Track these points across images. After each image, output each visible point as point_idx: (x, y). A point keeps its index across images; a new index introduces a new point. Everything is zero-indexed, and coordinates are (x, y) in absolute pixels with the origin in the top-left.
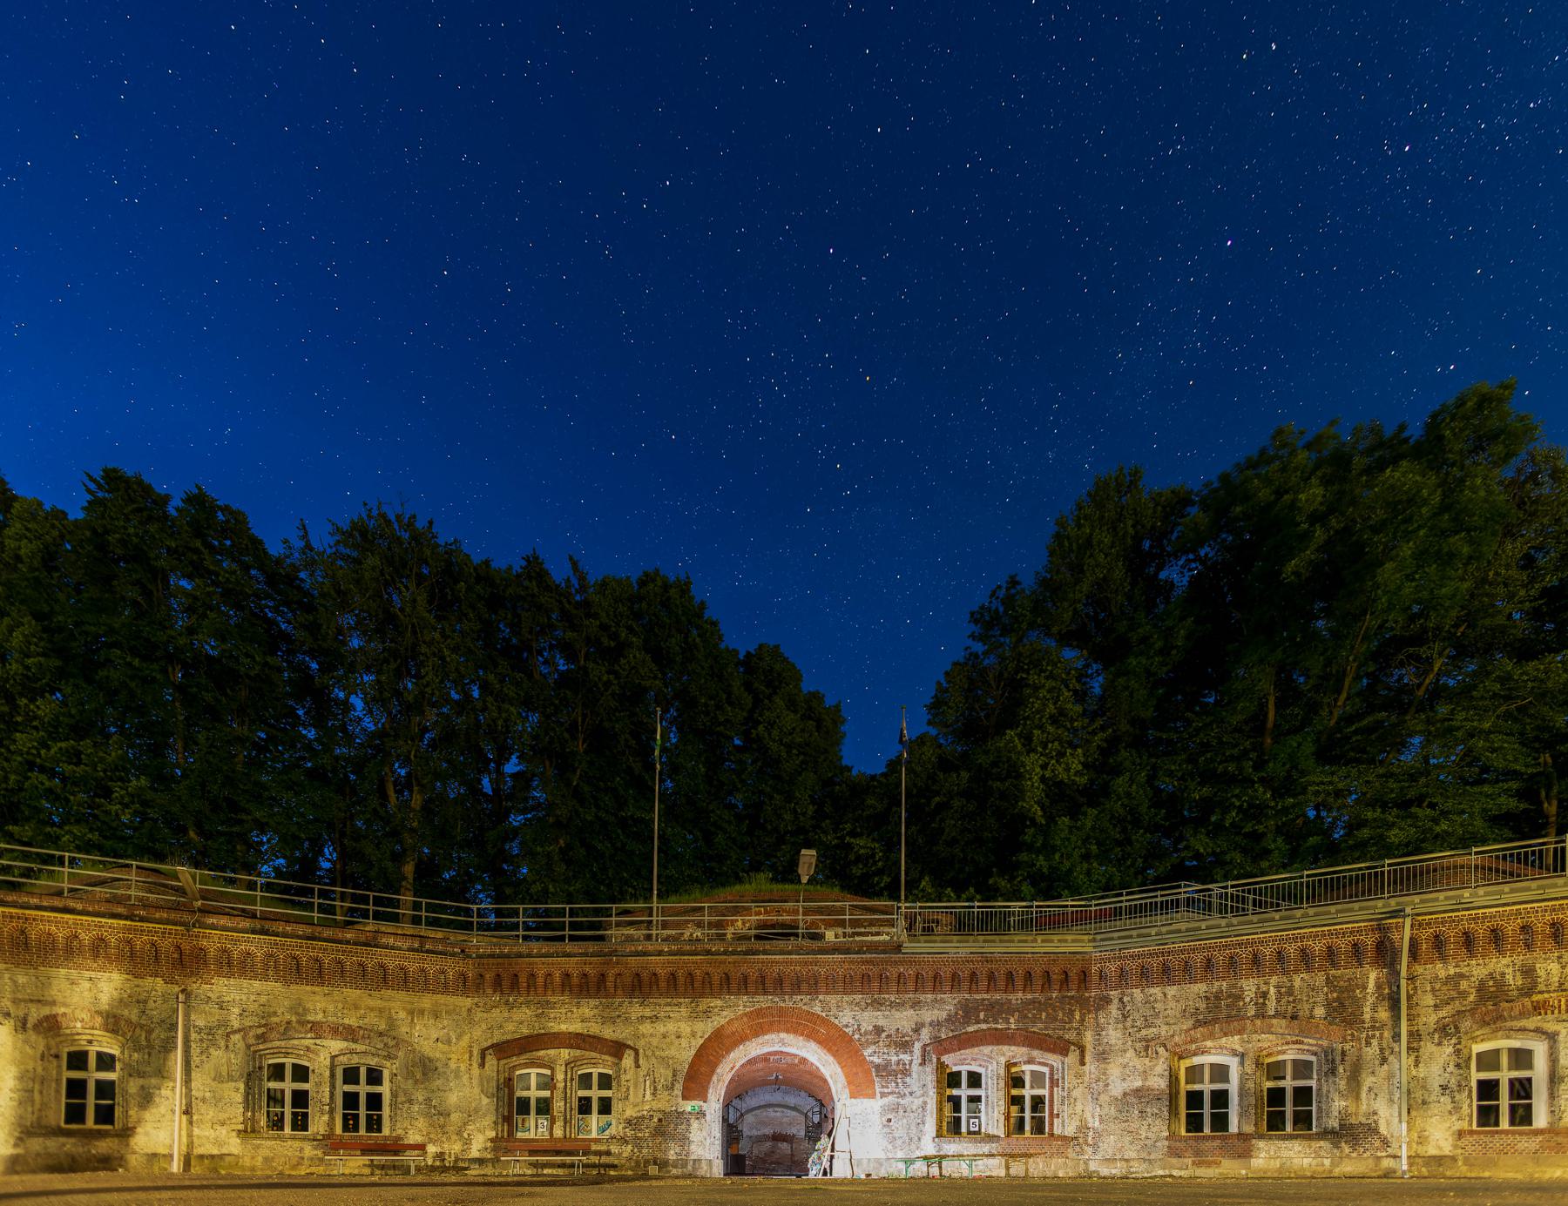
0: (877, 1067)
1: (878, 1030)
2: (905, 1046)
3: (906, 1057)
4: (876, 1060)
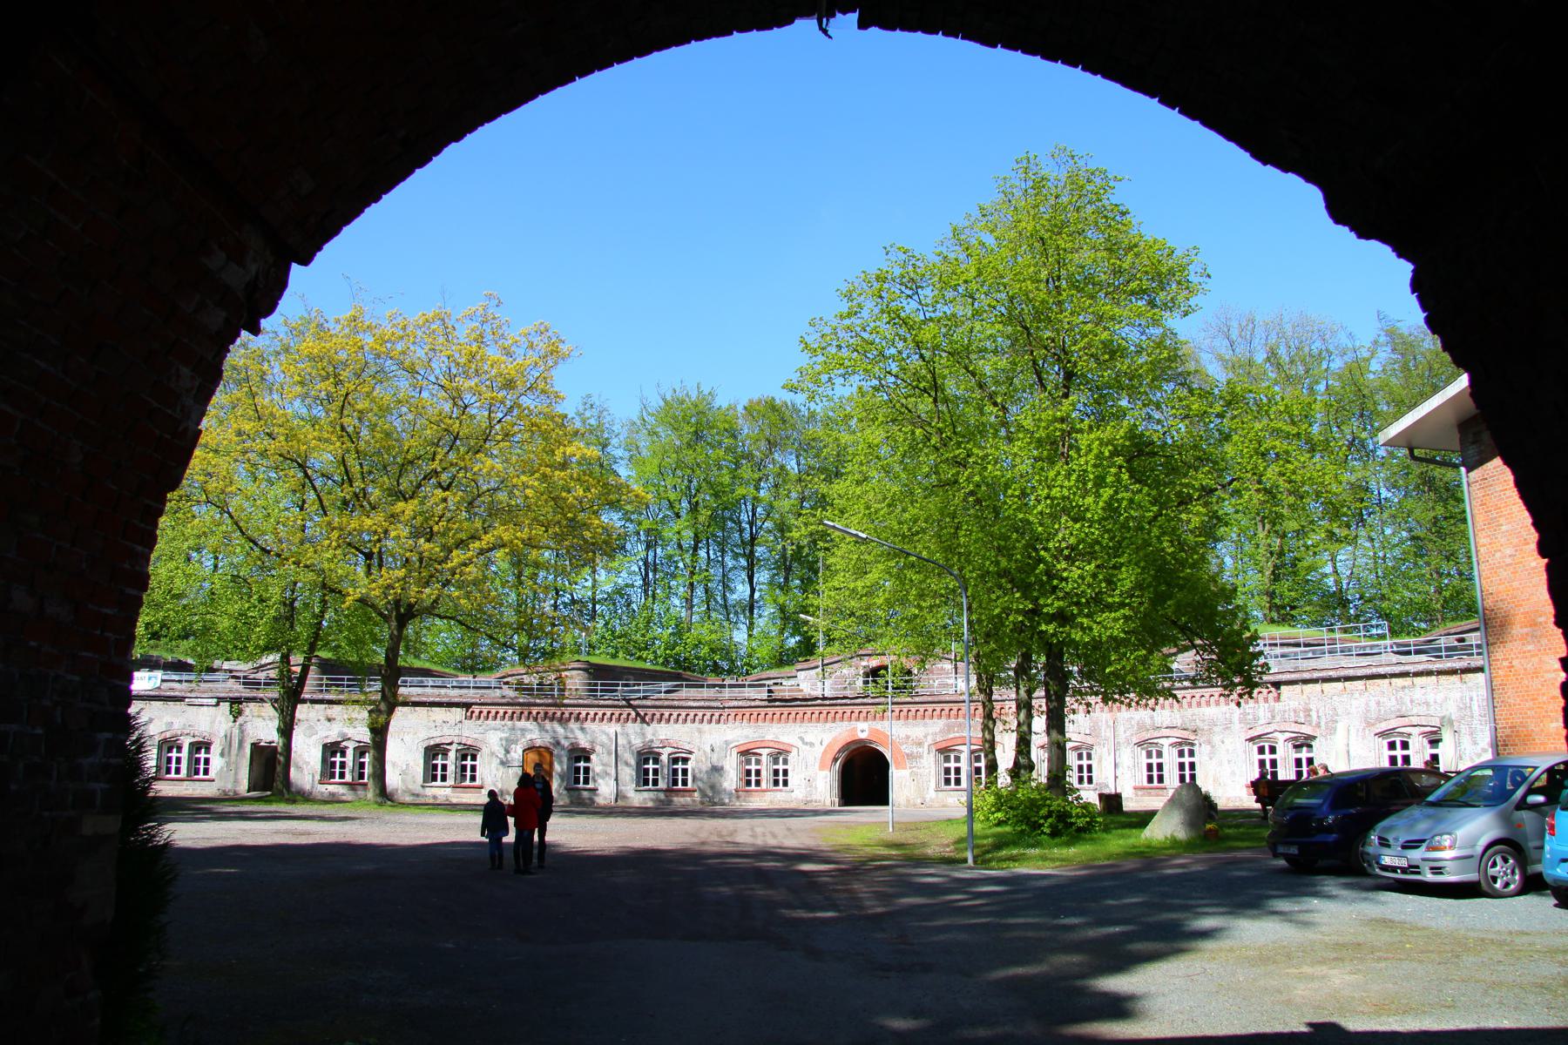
2: (920, 744)
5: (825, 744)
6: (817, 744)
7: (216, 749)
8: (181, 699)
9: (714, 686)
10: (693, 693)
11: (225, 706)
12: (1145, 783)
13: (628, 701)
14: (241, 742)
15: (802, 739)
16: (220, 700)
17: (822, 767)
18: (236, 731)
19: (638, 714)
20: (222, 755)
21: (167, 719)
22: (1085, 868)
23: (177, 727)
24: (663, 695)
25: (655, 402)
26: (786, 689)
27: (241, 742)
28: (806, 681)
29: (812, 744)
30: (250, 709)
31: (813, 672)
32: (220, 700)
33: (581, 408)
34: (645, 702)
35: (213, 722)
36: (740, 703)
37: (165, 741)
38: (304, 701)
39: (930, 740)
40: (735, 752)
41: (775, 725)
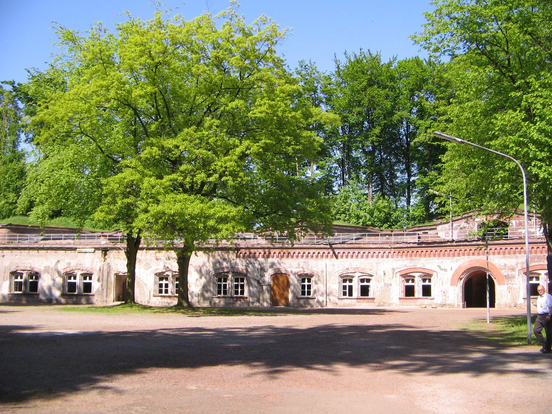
0: (505, 276)
1: (505, 265)
2: (513, 269)
3: (514, 273)
4: (505, 274)
5: (454, 270)
6: (449, 269)
7: (95, 277)
8: (75, 249)
9: (385, 235)
10: (373, 239)
11: (99, 253)
12: (158, 294)
13: (330, 244)
14: (109, 273)
15: (439, 266)
16: (96, 249)
17: (453, 283)
18: (106, 268)
19: (334, 253)
20: (99, 280)
21: (68, 261)
22: (106, 388)
23: (73, 264)
24: (354, 241)
25: (344, 62)
26: (430, 236)
27: (109, 273)
28: (443, 231)
29: (446, 270)
30: (112, 254)
31: (446, 226)
32: (96, 249)
33: (299, 69)
34: (343, 246)
35: (93, 262)
36: (401, 245)
37: (67, 273)
38: (142, 249)
39: (519, 267)
40: (398, 275)
41: (422, 258)
